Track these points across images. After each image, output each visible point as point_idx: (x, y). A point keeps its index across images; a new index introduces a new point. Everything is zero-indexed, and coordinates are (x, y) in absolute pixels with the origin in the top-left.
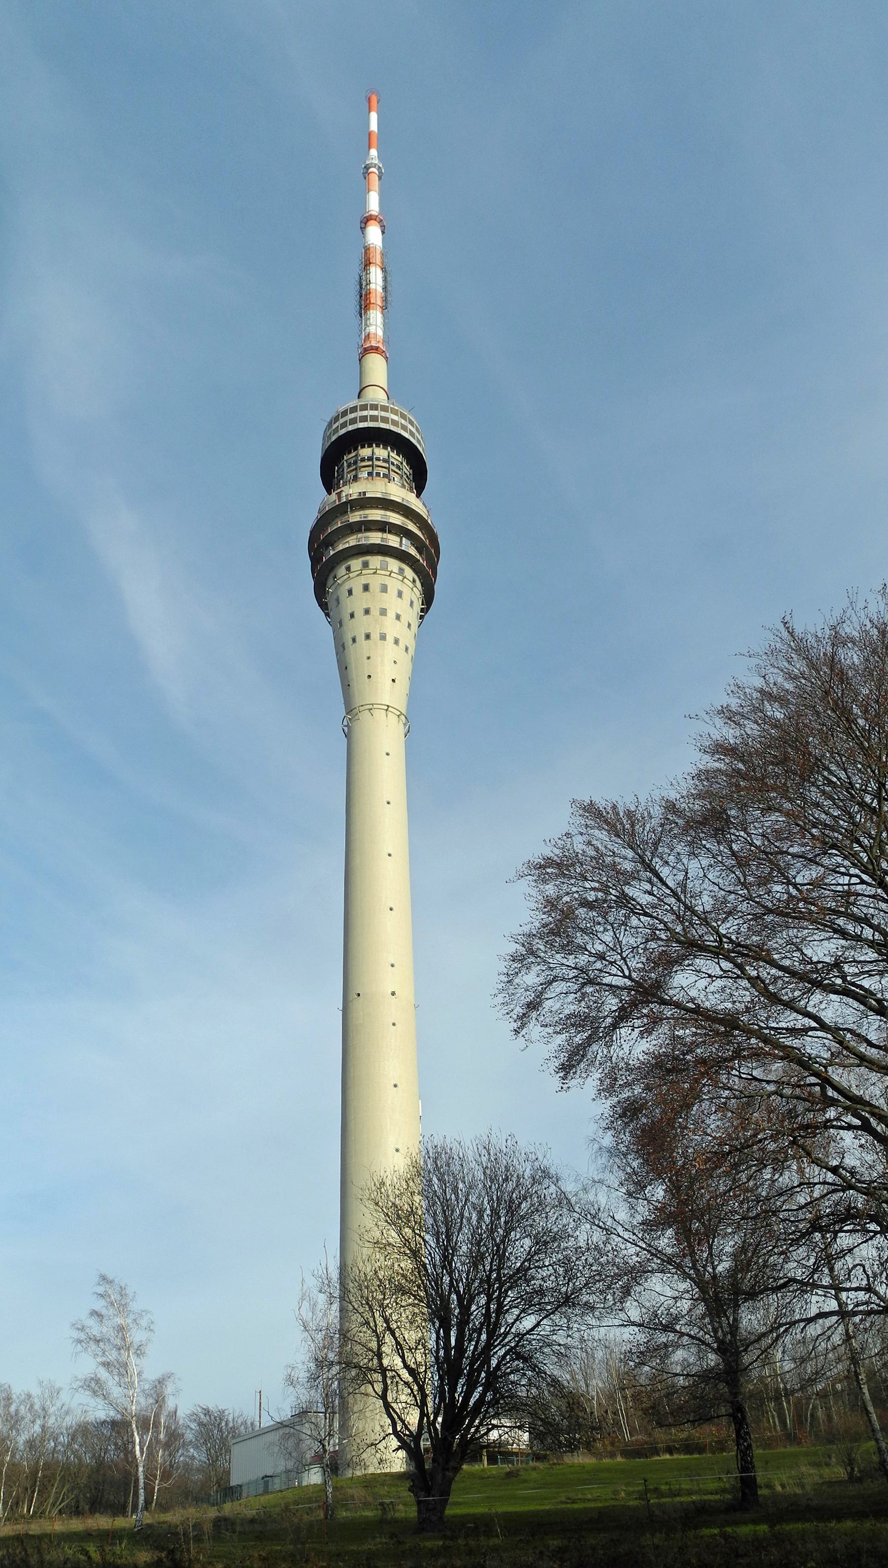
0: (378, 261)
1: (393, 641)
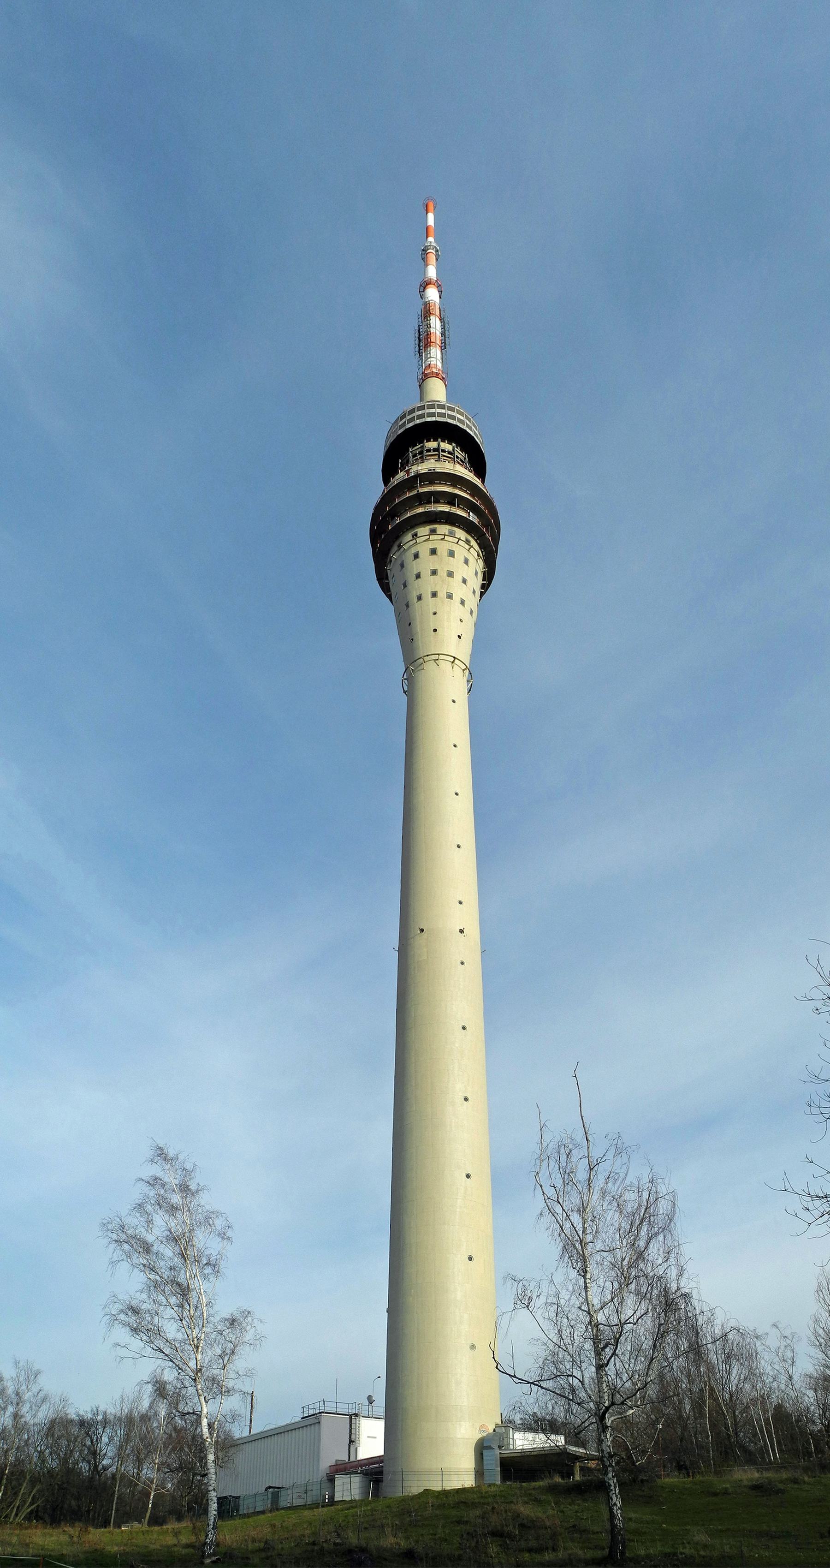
0: (438, 313)
1: (459, 601)
